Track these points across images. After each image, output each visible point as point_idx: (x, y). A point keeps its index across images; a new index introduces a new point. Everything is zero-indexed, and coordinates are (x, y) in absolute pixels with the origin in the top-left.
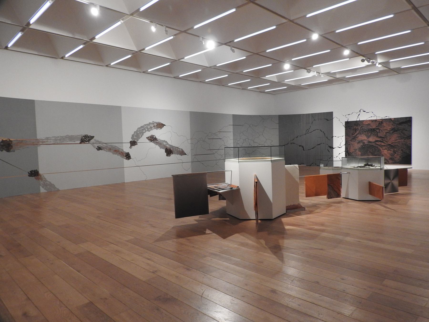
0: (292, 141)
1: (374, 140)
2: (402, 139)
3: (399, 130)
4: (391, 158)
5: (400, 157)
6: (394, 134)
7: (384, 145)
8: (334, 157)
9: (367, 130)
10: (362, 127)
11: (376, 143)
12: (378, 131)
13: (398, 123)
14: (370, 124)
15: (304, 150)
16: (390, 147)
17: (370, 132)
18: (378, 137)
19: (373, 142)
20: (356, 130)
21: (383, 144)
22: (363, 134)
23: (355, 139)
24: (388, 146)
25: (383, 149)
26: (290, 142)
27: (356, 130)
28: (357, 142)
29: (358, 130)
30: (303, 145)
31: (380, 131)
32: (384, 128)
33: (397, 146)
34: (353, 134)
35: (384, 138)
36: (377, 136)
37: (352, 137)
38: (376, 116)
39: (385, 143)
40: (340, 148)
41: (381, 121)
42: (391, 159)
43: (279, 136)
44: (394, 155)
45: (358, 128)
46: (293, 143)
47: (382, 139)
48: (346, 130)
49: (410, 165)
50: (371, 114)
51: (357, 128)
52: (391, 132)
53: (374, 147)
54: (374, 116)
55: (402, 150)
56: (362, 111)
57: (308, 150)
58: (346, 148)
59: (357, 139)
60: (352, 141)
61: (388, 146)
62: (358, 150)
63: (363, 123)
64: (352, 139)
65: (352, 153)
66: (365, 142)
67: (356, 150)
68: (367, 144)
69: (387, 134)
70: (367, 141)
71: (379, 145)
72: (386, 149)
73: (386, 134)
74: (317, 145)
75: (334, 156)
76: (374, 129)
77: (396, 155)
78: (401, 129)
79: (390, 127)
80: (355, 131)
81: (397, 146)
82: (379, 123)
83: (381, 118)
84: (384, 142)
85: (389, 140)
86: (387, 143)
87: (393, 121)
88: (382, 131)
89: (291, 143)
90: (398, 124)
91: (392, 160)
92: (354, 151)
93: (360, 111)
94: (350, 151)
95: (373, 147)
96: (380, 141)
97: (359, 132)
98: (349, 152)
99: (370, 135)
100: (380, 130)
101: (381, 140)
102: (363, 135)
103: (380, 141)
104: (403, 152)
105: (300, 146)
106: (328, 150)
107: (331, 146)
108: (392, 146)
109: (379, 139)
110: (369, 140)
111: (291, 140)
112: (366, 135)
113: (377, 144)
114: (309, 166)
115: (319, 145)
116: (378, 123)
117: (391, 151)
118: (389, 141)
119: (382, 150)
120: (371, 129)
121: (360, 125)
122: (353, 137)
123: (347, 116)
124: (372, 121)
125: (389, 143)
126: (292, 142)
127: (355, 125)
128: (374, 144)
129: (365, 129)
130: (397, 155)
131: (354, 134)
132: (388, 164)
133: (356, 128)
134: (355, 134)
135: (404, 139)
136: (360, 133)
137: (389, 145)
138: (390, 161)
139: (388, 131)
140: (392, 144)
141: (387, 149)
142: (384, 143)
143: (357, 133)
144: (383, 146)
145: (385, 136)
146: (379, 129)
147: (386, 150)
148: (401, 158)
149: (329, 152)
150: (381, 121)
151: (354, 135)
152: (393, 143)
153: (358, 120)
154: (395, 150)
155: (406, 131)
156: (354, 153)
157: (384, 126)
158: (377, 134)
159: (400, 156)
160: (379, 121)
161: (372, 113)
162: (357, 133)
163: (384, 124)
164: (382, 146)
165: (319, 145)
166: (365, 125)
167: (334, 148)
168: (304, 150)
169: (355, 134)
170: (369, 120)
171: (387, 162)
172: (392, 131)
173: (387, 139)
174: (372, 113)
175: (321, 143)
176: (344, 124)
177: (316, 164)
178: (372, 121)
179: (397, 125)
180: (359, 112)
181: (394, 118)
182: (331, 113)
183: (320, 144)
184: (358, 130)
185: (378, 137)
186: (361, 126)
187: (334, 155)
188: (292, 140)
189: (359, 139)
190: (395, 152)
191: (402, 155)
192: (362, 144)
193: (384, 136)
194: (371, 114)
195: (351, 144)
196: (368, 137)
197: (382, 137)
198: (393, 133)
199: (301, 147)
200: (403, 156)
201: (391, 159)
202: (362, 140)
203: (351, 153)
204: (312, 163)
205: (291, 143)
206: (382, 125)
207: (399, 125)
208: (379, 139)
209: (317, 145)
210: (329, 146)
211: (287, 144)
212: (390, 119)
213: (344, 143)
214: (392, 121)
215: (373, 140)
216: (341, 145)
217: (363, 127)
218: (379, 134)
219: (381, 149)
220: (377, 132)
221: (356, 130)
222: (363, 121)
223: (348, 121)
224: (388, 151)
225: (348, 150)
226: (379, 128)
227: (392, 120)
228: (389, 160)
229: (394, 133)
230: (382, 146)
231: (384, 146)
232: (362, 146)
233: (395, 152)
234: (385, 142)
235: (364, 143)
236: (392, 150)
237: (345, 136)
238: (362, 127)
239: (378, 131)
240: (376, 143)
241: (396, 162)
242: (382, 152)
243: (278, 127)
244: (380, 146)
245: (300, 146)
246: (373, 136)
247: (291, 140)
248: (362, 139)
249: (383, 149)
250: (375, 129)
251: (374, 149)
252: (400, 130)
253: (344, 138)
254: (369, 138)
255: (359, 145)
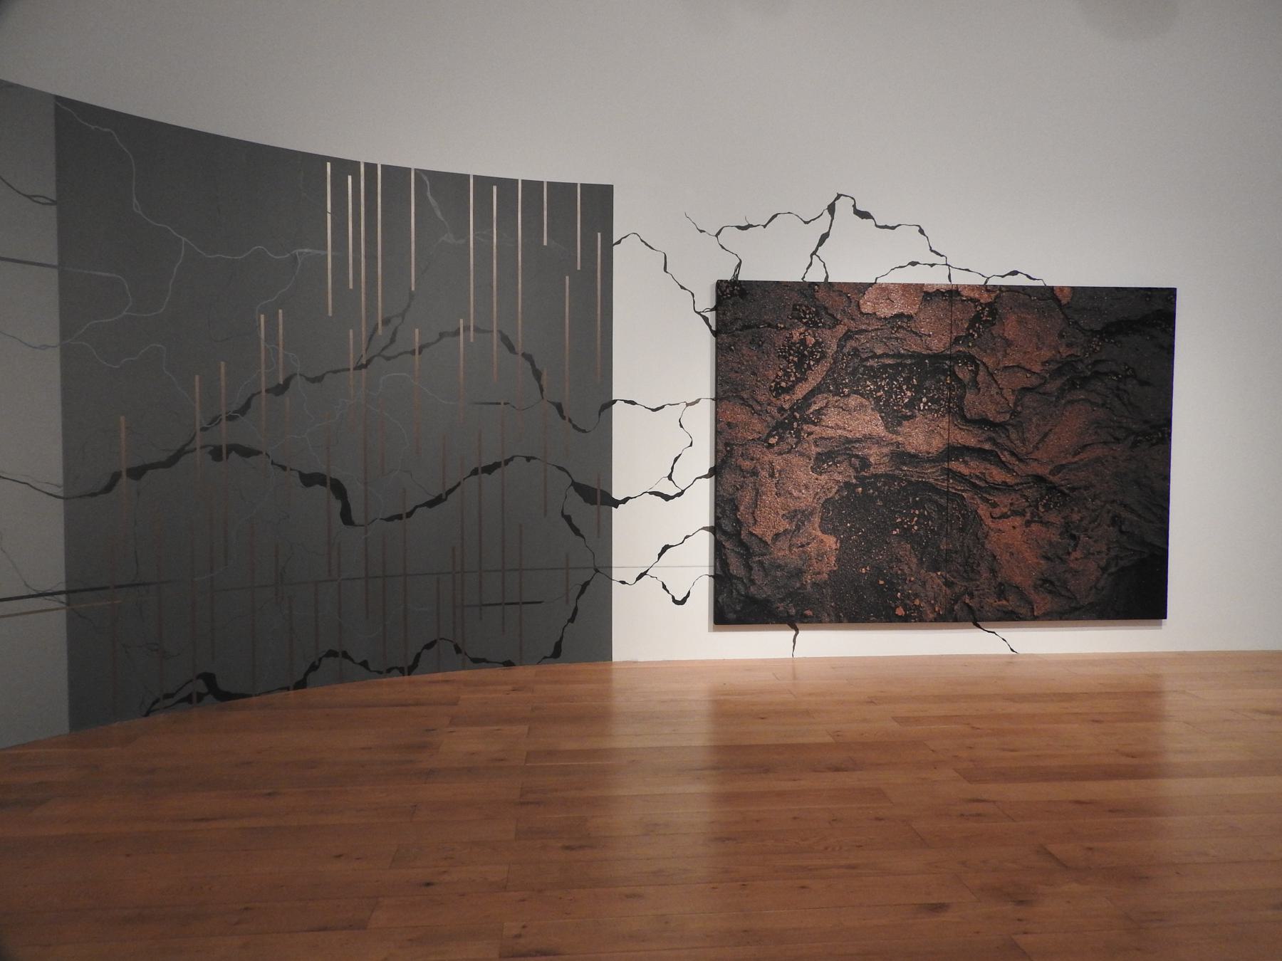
0: (502, 405)
1: (937, 444)
2: (1117, 440)
3: (1097, 375)
4: (1045, 581)
5: (1104, 569)
6: (1071, 402)
7: (1005, 483)
8: (617, 574)
9: (885, 366)
10: (848, 336)
11: (954, 465)
12: (964, 373)
13: (1097, 326)
14: (910, 317)
15: (346, 517)
16: (1042, 498)
17: (908, 380)
18: (964, 417)
19: (929, 460)
20: (802, 357)
21: (998, 475)
22: (856, 392)
23: (798, 432)
24: (1028, 493)
25: (997, 512)
26: (198, 443)
27: (802, 357)
28: (814, 450)
29: (823, 356)
30: (337, 473)
31: (982, 373)
32: (1006, 354)
33: (1086, 488)
34: (779, 391)
35: (1002, 426)
36: (962, 409)
37: (774, 411)
38: (942, 260)
39: (1010, 471)
40: (667, 498)
41: (985, 298)
42: (1046, 583)
43: (68, 356)
44: (1069, 554)
45: (817, 343)
46: (232, 448)
47: (990, 439)
48: (721, 351)
49: (1159, 627)
50: (908, 245)
51: (811, 340)
52: (1052, 387)
53: (936, 498)
54: (936, 259)
55: (1116, 521)
56: (843, 207)
57: (390, 519)
58: (724, 506)
59: (812, 428)
60: (770, 446)
61: (1028, 493)
62: (816, 520)
63: (858, 306)
64: (775, 428)
65: (768, 539)
66: (874, 454)
67: (806, 515)
68: (881, 470)
69: (1028, 400)
70: (885, 450)
71: (974, 485)
72: (1015, 513)
73: (1015, 404)
74: (475, 472)
75: (614, 571)
76: (937, 357)
77: (1078, 554)
78: (1116, 375)
79: (1046, 354)
80: (799, 366)
81: (1086, 488)
82: (977, 318)
83: (981, 281)
84: (1006, 457)
85: (1036, 447)
86: (1021, 465)
87: (1068, 305)
88: (991, 375)
89: (217, 454)
90: (1094, 332)
91: (1050, 592)
92: (785, 525)
93: (831, 209)
94: (757, 531)
95: (930, 500)
96: (980, 453)
97: (831, 370)
98: (751, 534)
99: (912, 399)
100: (977, 366)
101: (987, 446)
102: (854, 401)
103: (980, 453)
104: (1121, 532)
105: (310, 480)
106: (568, 519)
107: (593, 484)
108: (1053, 488)
109: (967, 438)
110: (898, 444)
111: (215, 420)
112: (878, 399)
113: (960, 477)
114: (402, 671)
115: (489, 469)
116: (963, 317)
117: (1046, 524)
118: (1037, 455)
119: (989, 521)
120: (918, 357)
121: (837, 322)
122: (781, 410)
123: (730, 236)
124: (927, 294)
125: (1035, 464)
126: (225, 434)
127: (797, 314)
128: (932, 474)
129: (875, 356)
130: (1088, 555)
131: (788, 390)
132: (1025, 620)
133: (803, 342)
134: (801, 391)
135: (1132, 438)
136: (833, 385)
137: (1039, 479)
138: (1043, 601)
139: (1034, 381)
140: (1052, 473)
141: (1023, 514)
142: (1003, 465)
143: (813, 380)
144: (994, 487)
145: (1014, 413)
146: (972, 359)
147: (1018, 519)
148: (1112, 574)
149: (576, 531)
150: (988, 304)
151: (786, 401)
152: (1063, 466)
153: (816, 276)
154: (1076, 517)
155: (1143, 383)
156: (783, 543)
157: (1008, 343)
158: (961, 398)
159: (1103, 563)
160: (972, 300)
161: (921, 231)
162: (813, 380)
163: (1010, 328)
164: (986, 489)
165: (489, 469)
166: (877, 325)
167: (616, 503)
168: (346, 517)
169: (801, 391)
170: (906, 288)
171: (1022, 611)
172: (1059, 383)
173: (1023, 441)
174: (921, 231)
175: (511, 459)
176: (707, 300)
177: (458, 650)
178: (928, 295)
179: (1090, 341)
180: (827, 215)
181: (1074, 289)
182: (600, 198)
183: (496, 466)
184: (818, 361)
185: (964, 417)
186: (841, 330)
187: (614, 564)
188: (230, 418)
189: (830, 433)
190: (1069, 532)
191: (1113, 553)
192: (842, 473)
193: (1000, 419)
194: (908, 245)
195: (764, 473)
196: (894, 418)
197: (993, 425)
198: (1062, 390)
199: (321, 492)
200: (1122, 563)
201: (1046, 583)
202: (849, 441)
203: (766, 543)
204: (429, 646)
205: (217, 454)
206: (996, 330)
207: (1102, 339)
208: (967, 438)
209: (475, 472)
210: (576, 480)
211: (163, 457)
212: (1048, 294)
213: (703, 457)
214: (1060, 306)
215: (930, 444)
216: (682, 479)
217: (863, 338)
218: (970, 396)
219: (983, 510)
220: (959, 380)
221: (802, 357)
222: (862, 288)
223: (735, 282)
224: (1028, 523)
225: (738, 521)
226: (973, 351)
227: (1058, 301)
228: (1034, 596)
229: (1069, 397)
230: (986, 489)
231: (1006, 488)
232: (847, 485)
233: (1073, 537)
234: (1013, 460)
235: (865, 463)
236: (1054, 517)
237: (718, 399)
238: (848, 336)
239: (964, 373)
240: (954, 465)
241: (1076, 609)
242: (986, 536)
243: (48, 251)
244: (980, 488)
245: (310, 480)
246: (930, 410)
247: (215, 420)
248: (845, 433)
249: (997, 512)
250: (950, 357)
251: (934, 515)
252: (1106, 374)
253: (702, 422)
254: (900, 424)
255: (824, 477)
